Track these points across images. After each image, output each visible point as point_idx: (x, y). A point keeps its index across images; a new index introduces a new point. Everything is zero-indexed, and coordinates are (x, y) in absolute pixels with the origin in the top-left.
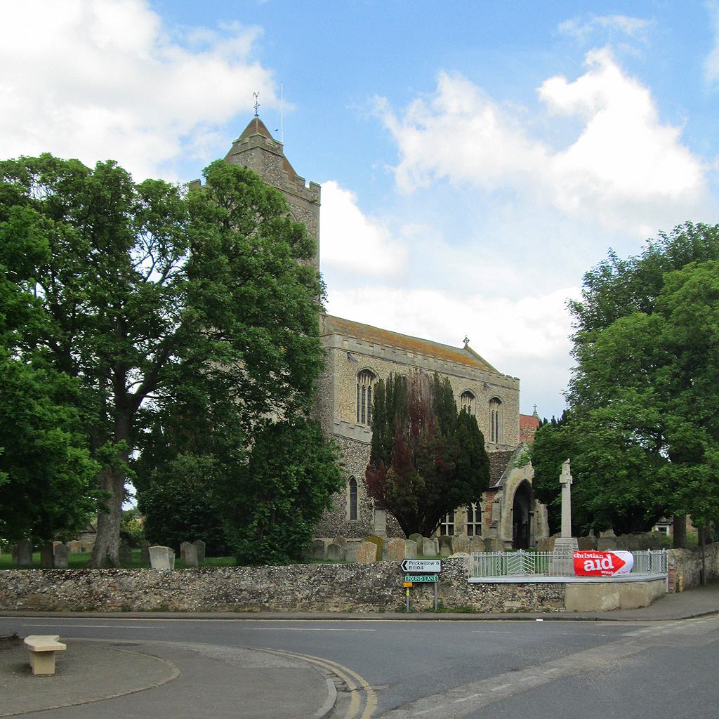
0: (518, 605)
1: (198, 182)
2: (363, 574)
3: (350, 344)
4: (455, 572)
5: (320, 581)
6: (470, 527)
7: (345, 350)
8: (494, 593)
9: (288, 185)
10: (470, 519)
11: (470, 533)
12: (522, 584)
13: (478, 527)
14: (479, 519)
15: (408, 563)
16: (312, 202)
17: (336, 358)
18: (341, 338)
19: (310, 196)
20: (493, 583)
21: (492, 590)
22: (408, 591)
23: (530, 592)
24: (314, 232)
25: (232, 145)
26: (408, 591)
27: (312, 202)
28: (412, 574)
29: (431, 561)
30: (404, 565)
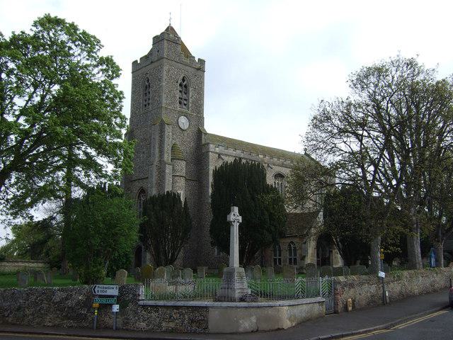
0: (172, 325)
1: (137, 61)
2: (71, 295)
5: (43, 300)
6: (290, 259)
7: (216, 153)
8: (157, 314)
10: (290, 255)
11: (290, 263)
13: (295, 259)
14: (295, 255)
17: (211, 158)
19: (198, 66)
22: (96, 311)
25: (196, 50)
26: (96, 311)
27: (199, 69)
28: (100, 296)
29: (112, 286)
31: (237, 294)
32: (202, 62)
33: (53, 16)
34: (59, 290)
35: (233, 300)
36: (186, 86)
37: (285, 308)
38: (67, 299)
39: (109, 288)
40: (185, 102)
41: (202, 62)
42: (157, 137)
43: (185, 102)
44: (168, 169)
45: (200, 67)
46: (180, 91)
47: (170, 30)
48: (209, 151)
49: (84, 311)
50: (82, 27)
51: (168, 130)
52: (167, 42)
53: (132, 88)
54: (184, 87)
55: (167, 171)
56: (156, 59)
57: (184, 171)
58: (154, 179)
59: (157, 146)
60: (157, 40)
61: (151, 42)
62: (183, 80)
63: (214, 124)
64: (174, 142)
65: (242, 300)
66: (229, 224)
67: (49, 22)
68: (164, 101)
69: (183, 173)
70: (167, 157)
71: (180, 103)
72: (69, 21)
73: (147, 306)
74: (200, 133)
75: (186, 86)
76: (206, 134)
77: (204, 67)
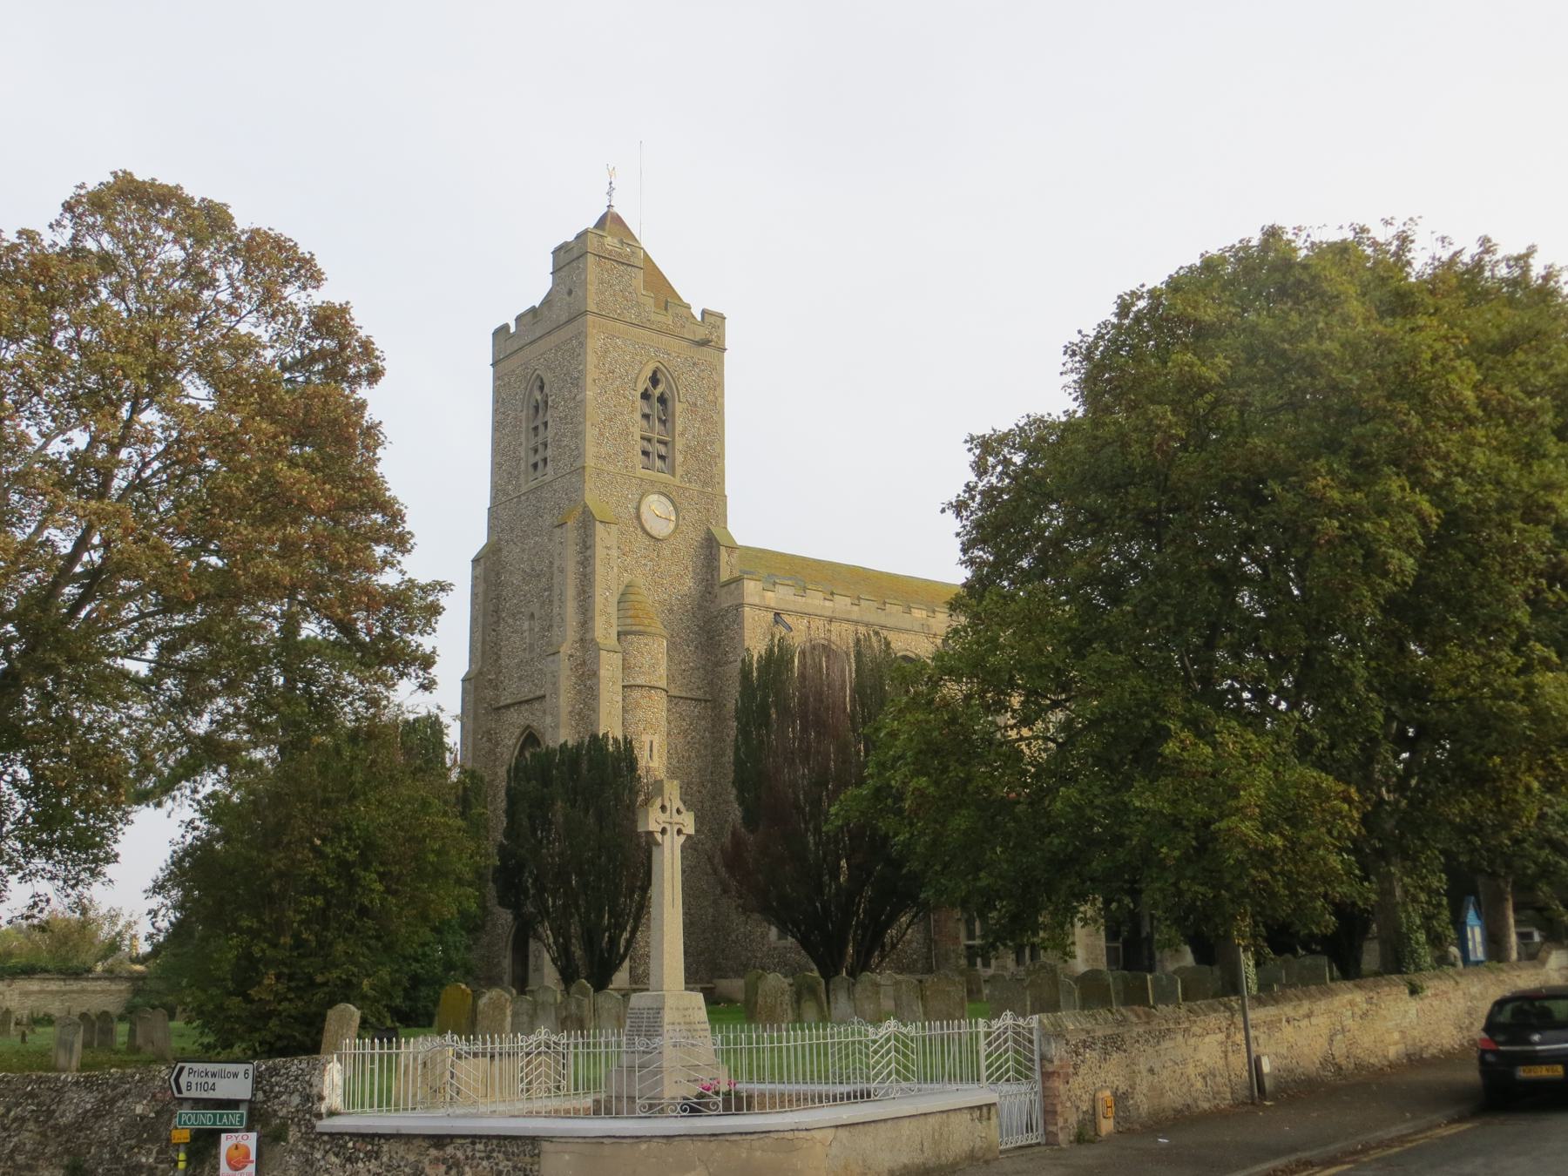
3: (780, 596)
4: (296, 1099)
7: (768, 608)
9: (653, 317)
12: (439, 1141)
15: (185, 1072)
16: (704, 343)
17: (748, 623)
18: (760, 585)
19: (701, 334)
20: (373, 1136)
21: (370, 1156)
23: (457, 1164)
24: (711, 398)
25: (696, 295)
27: (704, 343)
30: (177, 1080)
31: (675, 1088)
32: (714, 320)
33: (140, 176)
34: (77, 1083)
35: (654, 1109)
36: (662, 400)
37: (818, 1135)
38: (97, 1115)
39: (223, 1075)
40: (663, 450)
41: (714, 320)
42: (571, 567)
43: (663, 450)
44: (609, 668)
45: (708, 336)
46: (646, 416)
47: (610, 222)
48: (742, 605)
49: (149, 1152)
50: (244, 220)
51: (604, 538)
52: (599, 267)
53: (495, 411)
54: (658, 399)
55: (602, 673)
56: (564, 318)
57: (662, 670)
58: (565, 699)
59: (571, 592)
60: (568, 259)
61: (548, 265)
62: (655, 380)
63: (757, 517)
64: (627, 577)
65: (694, 1109)
66: (648, 845)
67: (127, 199)
68: (591, 450)
69: (660, 677)
70: (604, 629)
71: (645, 453)
72: (196, 191)
73: (342, 1135)
74: (711, 546)
75: (662, 400)
76: (733, 548)
77: (721, 337)
